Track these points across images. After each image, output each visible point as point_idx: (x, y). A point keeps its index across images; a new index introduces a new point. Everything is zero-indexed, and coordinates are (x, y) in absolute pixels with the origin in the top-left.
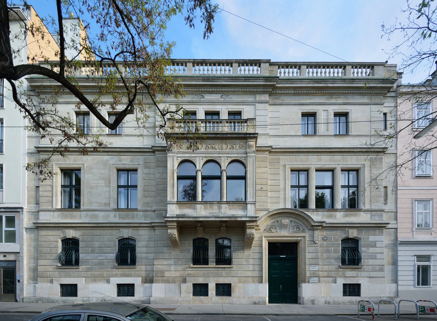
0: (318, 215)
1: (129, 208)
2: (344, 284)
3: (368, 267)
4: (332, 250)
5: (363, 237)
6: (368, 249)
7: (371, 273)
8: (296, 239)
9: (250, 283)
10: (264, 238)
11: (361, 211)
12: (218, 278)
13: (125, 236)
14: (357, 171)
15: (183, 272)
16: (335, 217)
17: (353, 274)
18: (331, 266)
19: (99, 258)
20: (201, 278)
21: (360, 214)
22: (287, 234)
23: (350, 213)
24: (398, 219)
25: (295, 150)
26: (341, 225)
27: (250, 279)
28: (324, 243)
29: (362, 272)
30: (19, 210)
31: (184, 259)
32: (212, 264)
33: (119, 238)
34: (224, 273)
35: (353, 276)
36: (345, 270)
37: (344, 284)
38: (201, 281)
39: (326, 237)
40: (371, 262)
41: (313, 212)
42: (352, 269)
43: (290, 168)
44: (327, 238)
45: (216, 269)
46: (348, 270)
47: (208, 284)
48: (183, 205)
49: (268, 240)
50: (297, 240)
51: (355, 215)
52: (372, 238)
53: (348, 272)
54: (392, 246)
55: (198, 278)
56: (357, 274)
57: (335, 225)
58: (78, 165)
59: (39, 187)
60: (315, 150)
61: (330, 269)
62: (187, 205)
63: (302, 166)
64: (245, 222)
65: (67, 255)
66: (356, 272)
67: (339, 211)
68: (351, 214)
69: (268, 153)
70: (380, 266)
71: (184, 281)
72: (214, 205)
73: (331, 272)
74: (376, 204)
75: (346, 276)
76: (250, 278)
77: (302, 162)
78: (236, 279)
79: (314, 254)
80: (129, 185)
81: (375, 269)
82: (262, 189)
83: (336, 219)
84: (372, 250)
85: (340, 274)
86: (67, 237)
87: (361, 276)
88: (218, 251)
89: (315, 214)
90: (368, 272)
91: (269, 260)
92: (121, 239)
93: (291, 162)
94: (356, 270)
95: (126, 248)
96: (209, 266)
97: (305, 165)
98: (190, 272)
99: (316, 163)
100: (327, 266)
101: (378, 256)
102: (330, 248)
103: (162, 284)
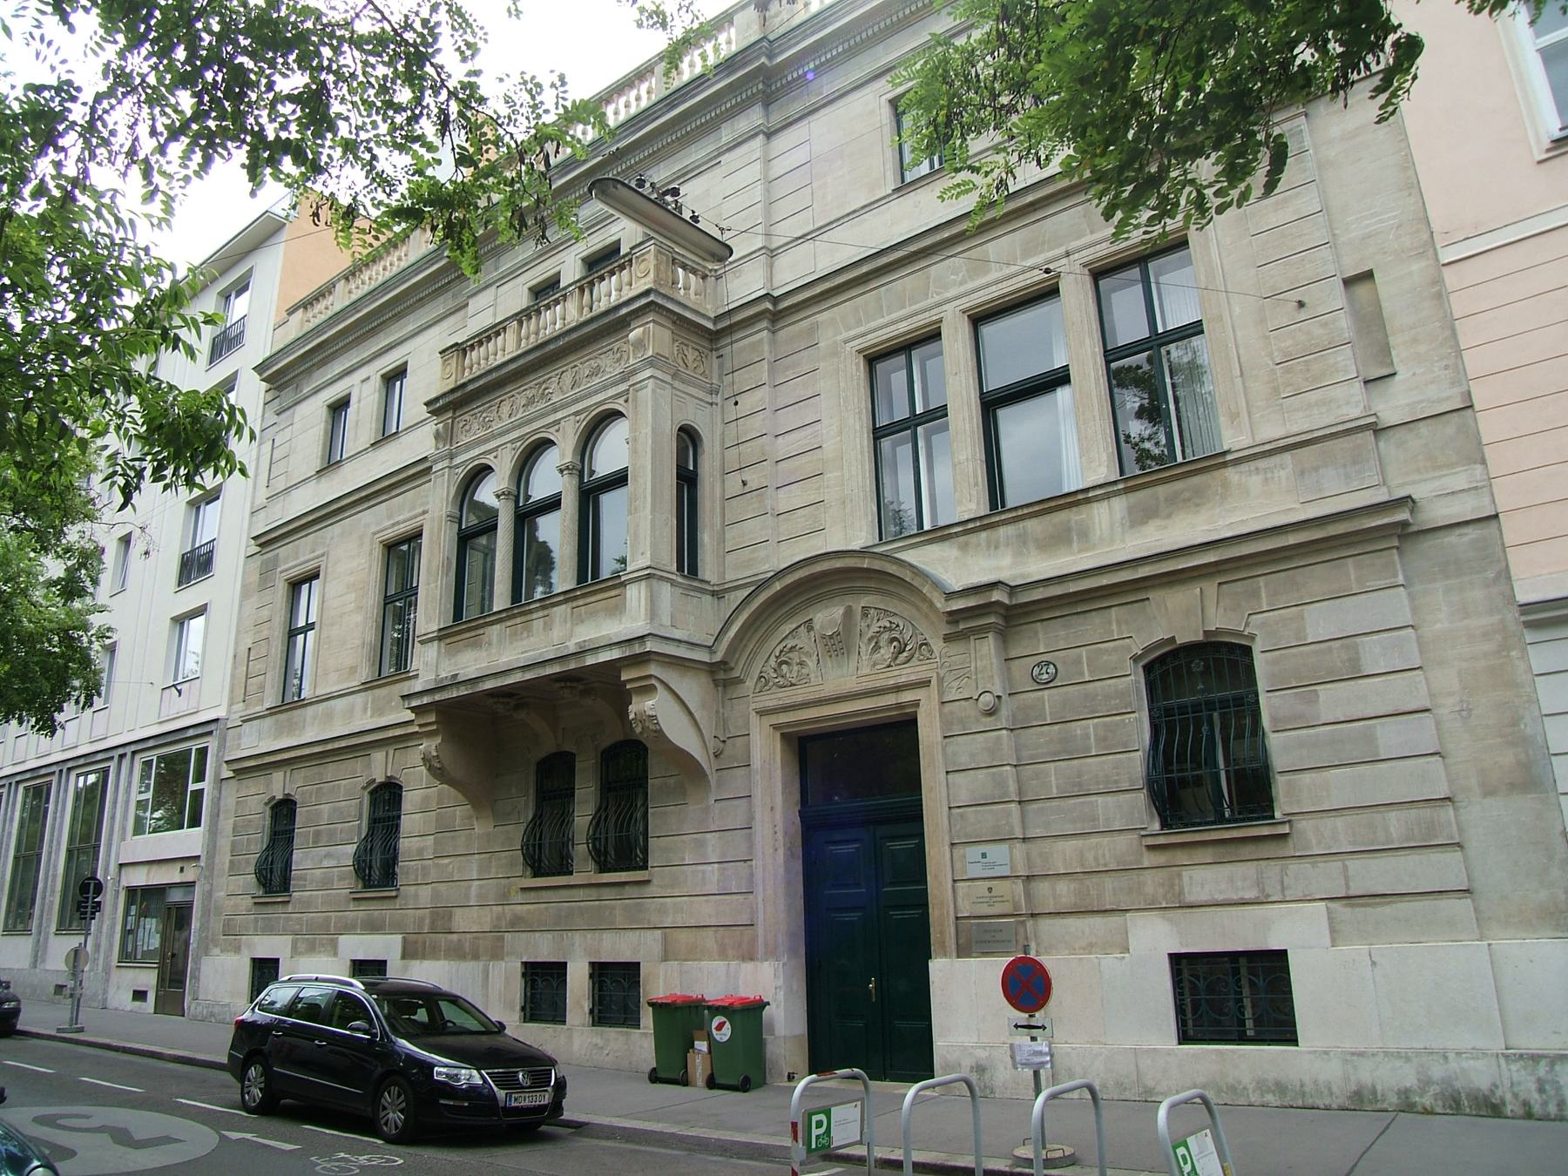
0: (996, 548)
1: (927, 526)
2: (1176, 959)
3: (1329, 823)
4: (1087, 736)
5: (1264, 624)
6: (1313, 699)
7: (1354, 864)
8: (890, 700)
9: (711, 959)
10: (754, 718)
11: (1225, 465)
12: (597, 933)
13: (1188, 634)
14: (873, 359)
15: (500, 908)
16: (1084, 535)
17: (1231, 880)
18: (1094, 840)
19: (326, 863)
20: (545, 934)
21: (1225, 485)
22: (850, 684)
23: (1161, 490)
24: (1488, 452)
25: (865, 269)
26: (1105, 580)
27: (709, 939)
28: (1042, 700)
29: (1293, 867)
30: (212, 727)
31: (504, 854)
32: (584, 872)
33: (1147, 650)
34: (617, 907)
35: (1235, 897)
36: (1181, 857)
37: (1176, 959)
38: (544, 950)
39: (1048, 663)
40: (1339, 787)
41: (973, 538)
42: (1221, 849)
43: (859, 352)
44: (1052, 669)
45: (593, 893)
46: (1206, 855)
47: (565, 964)
48: (459, 638)
49: (776, 727)
50: (900, 706)
51: (1196, 500)
52: (1321, 622)
53: (1199, 874)
54: (1490, 647)
55: (537, 934)
56: (1259, 883)
57: (1073, 587)
58: (994, 288)
59: (1368, 276)
60: (946, 235)
61: (1090, 856)
62: (468, 635)
63: (904, 324)
64: (613, 666)
65: (622, 824)
66: (1250, 869)
67: (1097, 499)
68: (1172, 500)
69: (765, 324)
70: (1413, 813)
71: (497, 953)
72: (535, 616)
73: (1095, 879)
74: (1314, 396)
75: (1190, 898)
76: (710, 931)
77: (903, 307)
78: (653, 940)
79: (981, 774)
80: (1160, 331)
81: (1102, 861)
82: (747, 489)
83: (1093, 547)
84: (1333, 701)
85: (1149, 889)
86: (1180, 641)
87: (1289, 895)
88: (1171, 732)
89: (984, 544)
90: (1335, 866)
91: (918, 817)
92: (1161, 659)
93: (859, 323)
94: (1247, 851)
95: (1196, 707)
96: (574, 879)
97: (916, 314)
98: (519, 907)
99: (962, 289)
100: (1073, 843)
101: (1389, 737)
102: (1077, 728)
103: (446, 962)
